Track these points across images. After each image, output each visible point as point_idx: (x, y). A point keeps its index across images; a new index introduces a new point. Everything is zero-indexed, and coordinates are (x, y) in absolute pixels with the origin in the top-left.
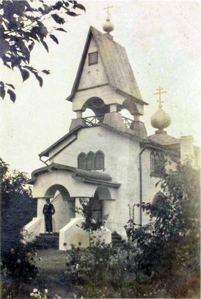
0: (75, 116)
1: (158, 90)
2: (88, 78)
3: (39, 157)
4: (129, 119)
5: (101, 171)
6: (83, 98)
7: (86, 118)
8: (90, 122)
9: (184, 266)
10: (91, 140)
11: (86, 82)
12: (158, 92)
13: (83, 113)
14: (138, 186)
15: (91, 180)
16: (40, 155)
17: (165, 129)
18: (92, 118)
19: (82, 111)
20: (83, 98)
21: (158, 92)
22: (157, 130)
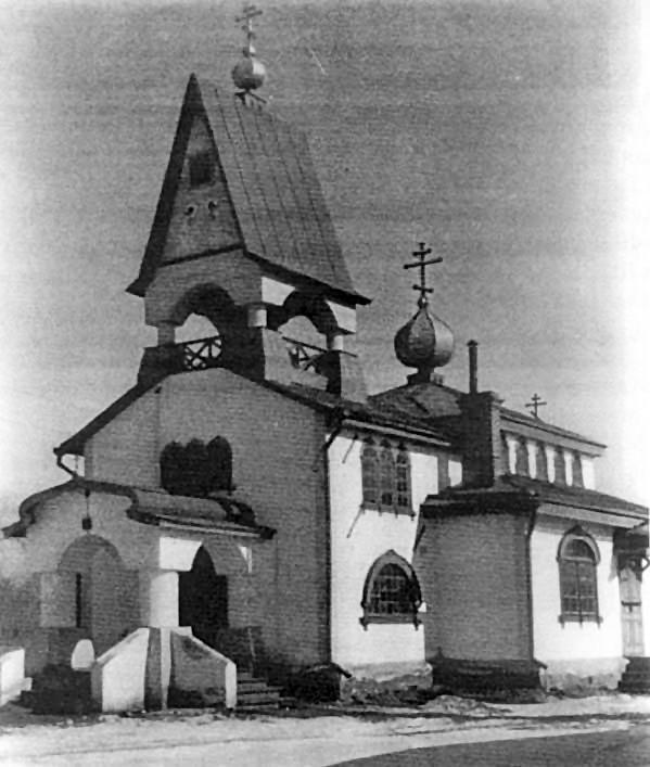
0: (151, 337)
1: (415, 254)
2: (185, 227)
3: (55, 457)
4: (192, 343)
5: (47, 590)
6: (174, 283)
7: (185, 344)
8: (197, 355)
9: (497, 458)
10: (197, 409)
11: (184, 239)
12: (417, 260)
13: (177, 330)
14: (480, 372)
15: (185, 524)
16: (59, 452)
17: (438, 371)
18: (200, 345)
19: (176, 320)
20: (174, 283)
21: (417, 260)
22: (414, 371)
